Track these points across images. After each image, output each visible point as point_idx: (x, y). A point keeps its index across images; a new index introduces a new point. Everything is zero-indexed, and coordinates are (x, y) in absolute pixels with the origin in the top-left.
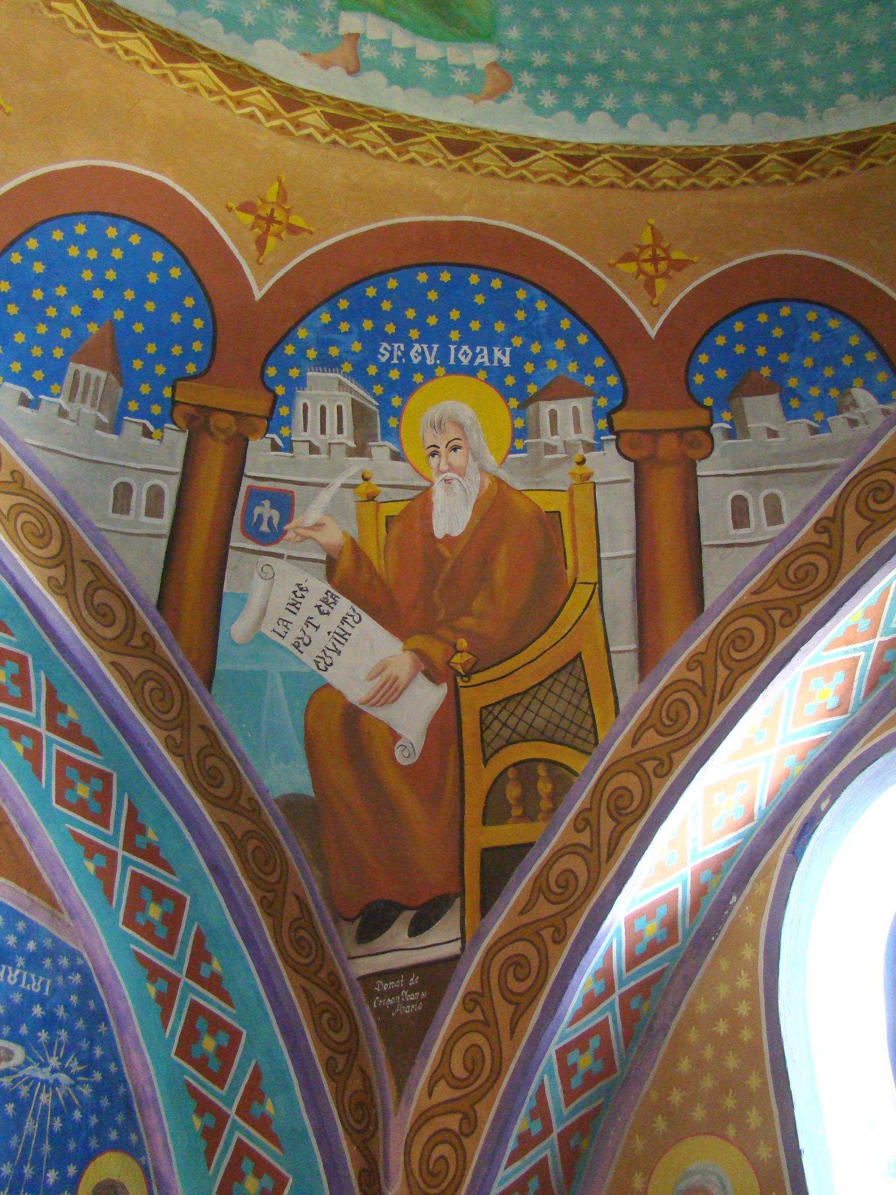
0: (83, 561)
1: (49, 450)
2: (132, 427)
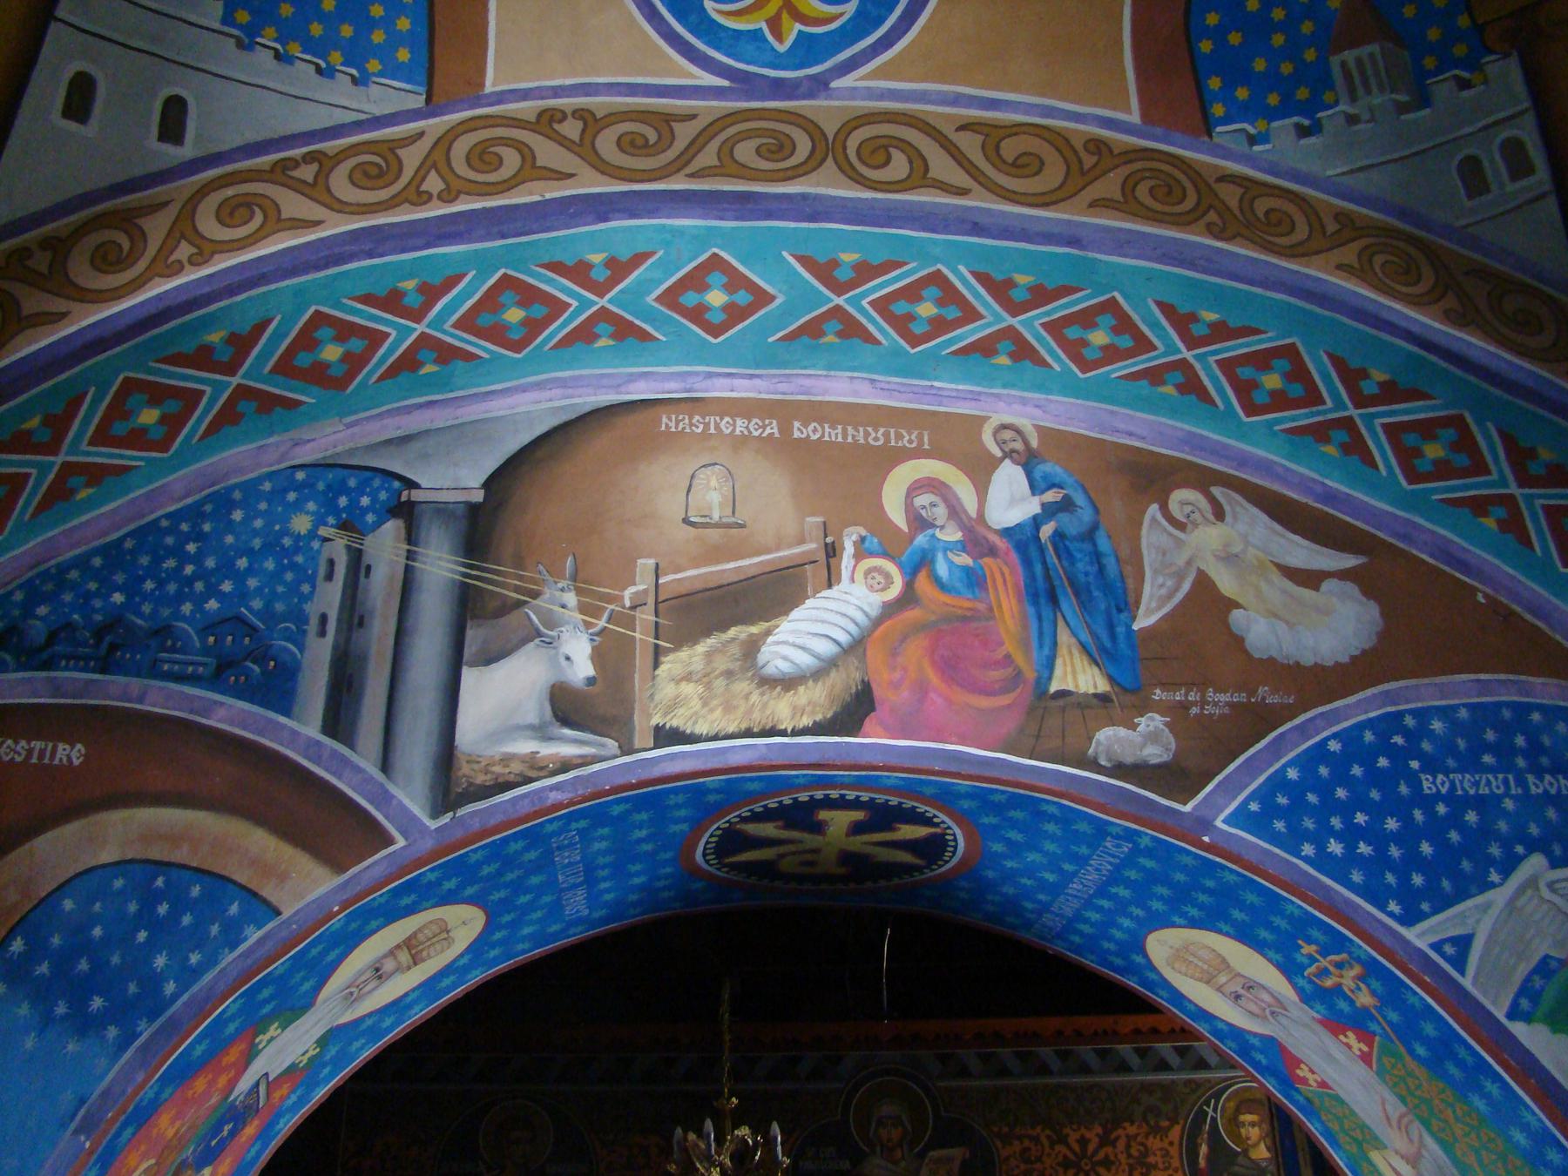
0: (1467, 273)
1: (1361, 169)
2: (1442, 89)
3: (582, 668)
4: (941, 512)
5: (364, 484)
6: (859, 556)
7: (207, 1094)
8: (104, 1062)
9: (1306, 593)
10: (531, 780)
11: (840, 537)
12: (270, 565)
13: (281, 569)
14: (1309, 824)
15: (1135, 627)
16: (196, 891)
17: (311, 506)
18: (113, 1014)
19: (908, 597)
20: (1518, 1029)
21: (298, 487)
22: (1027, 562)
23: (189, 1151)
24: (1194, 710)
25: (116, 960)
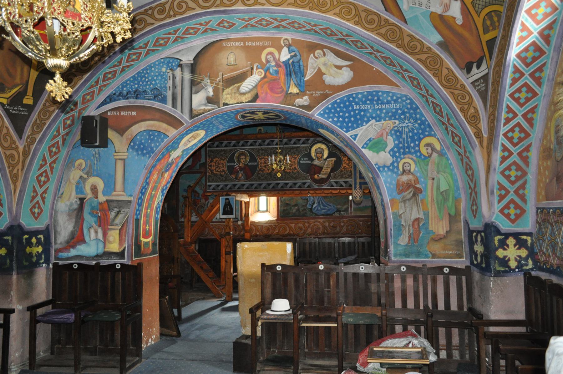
3: (211, 93)
4: (272, 59)
5: (173, 61)
6: (257, 69)
7: (164, 162)
8: (147, 160)
9: (339, 71)
10: (204, 113)
11: (253, 65)
12: (160, 78)
13: (162, 79)
14: (331, 115)
15: (305, 80)
16: (156, 134)
17: (165, 66)
18: (147, 153)
19: (265, 77)
20: (363, 150)
21: (162, 63)
22: (287, 68)
23: (163, 170)
24: (314, 95)
25: (146, 145)
